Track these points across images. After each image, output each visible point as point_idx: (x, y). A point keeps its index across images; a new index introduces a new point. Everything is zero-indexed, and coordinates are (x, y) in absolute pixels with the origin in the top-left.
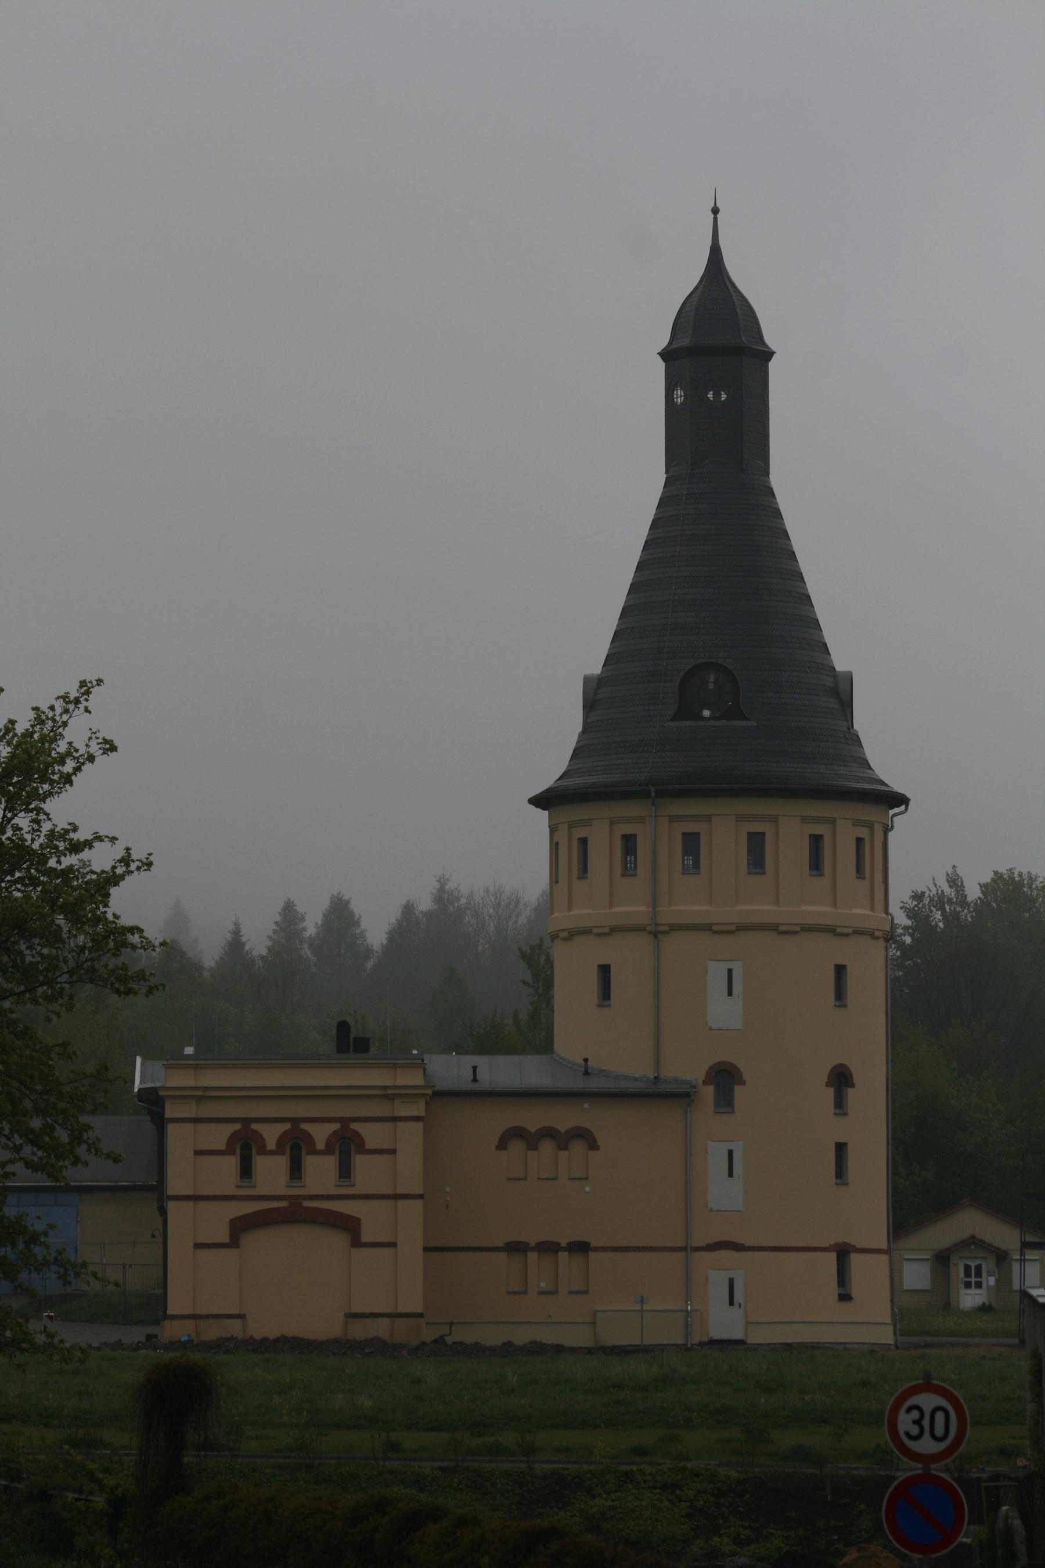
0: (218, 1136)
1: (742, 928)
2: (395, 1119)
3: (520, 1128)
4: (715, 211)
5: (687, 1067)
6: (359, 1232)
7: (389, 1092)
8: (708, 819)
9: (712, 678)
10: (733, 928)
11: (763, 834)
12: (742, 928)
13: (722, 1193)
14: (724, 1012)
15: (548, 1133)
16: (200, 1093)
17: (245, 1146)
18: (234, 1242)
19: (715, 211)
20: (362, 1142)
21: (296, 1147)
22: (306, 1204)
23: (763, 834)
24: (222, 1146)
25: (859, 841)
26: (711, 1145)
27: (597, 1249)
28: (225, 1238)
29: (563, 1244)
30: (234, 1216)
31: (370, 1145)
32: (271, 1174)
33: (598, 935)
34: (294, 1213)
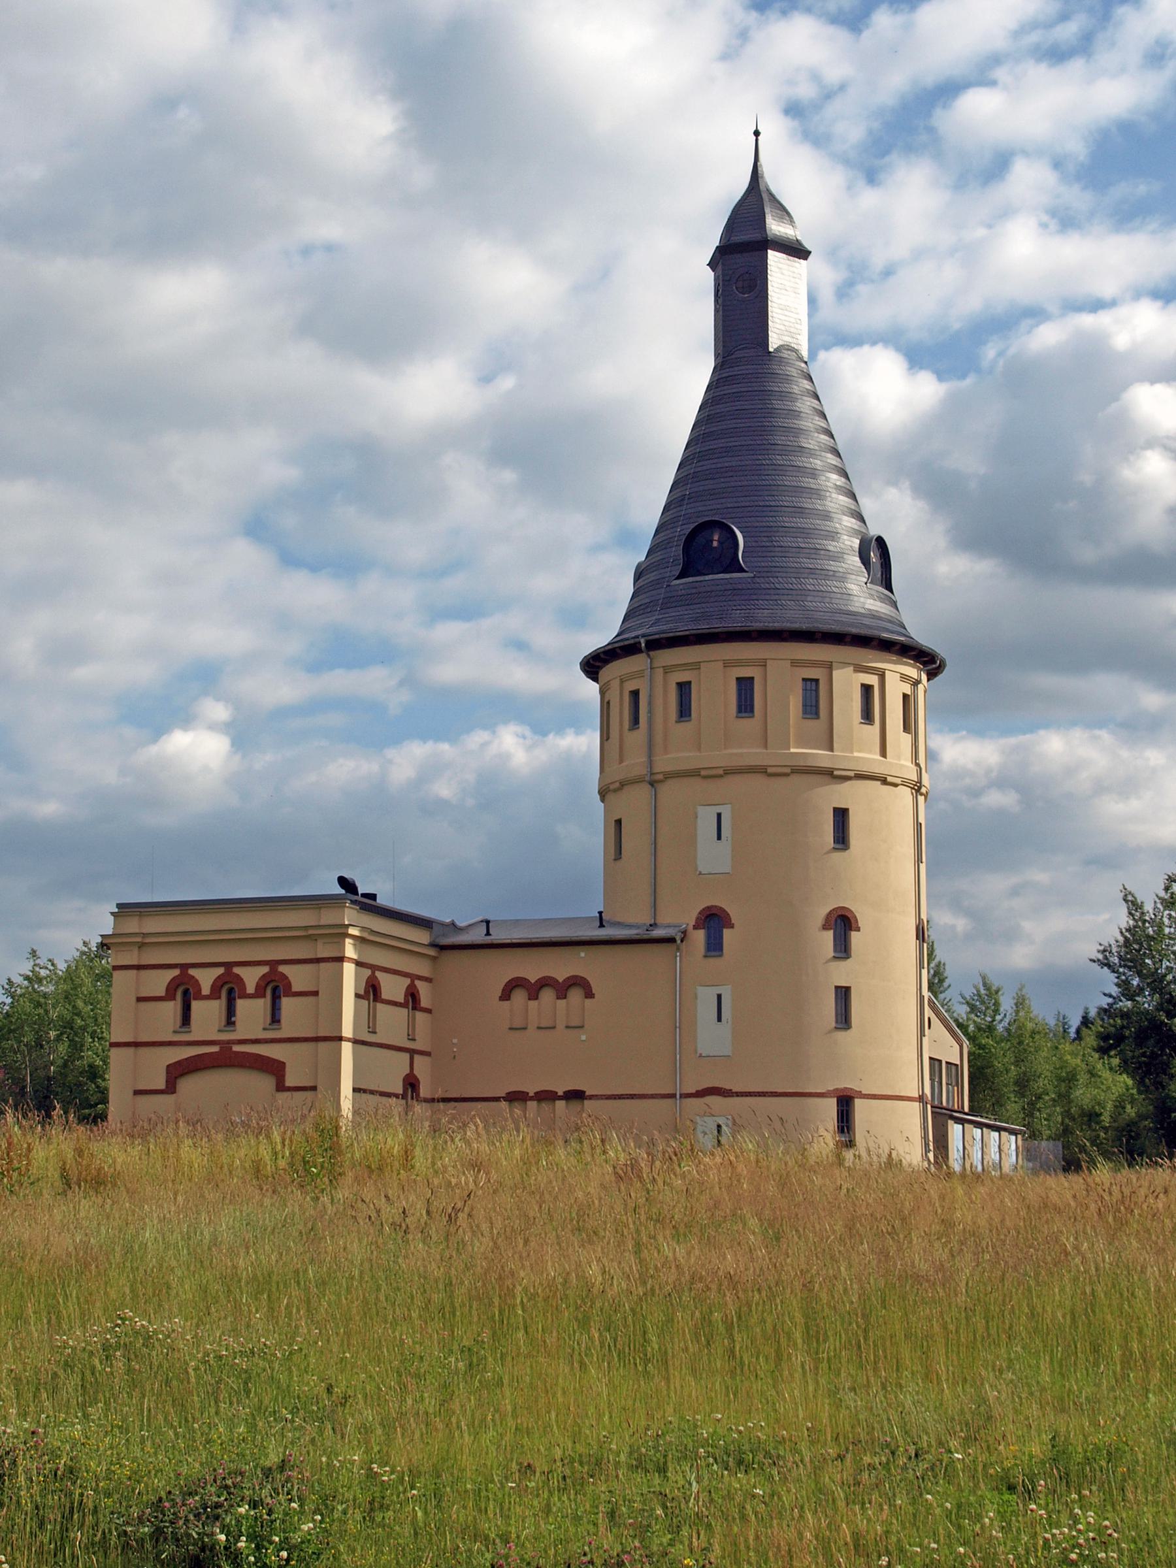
0: (158, 982)
1: (729, 772)
2: (318, 961)
3: (544, 978)
4: (757, 133)
5: (679, 914)
6: (284, 1076)
7: (311, 932)
8: (696, 666)
9: (716, 537)
10: (721, 772)
11: (752, 679)
12: (729, 772)
13: (712, 1038)
14: (713, 856)
15: (545, 982)
16: (139, 940)
17: (184, 991)
18: (171, 1088)
19: (757, 133)
20: (289, 985)
21: (229, 989)
22: (237, 1048)
23: (752, 679)
24: (162, 993)
25: (867, 689)
26: (700, 989)
27: (591, 1097)
28: (161, 1084)
29: (560, 1093)
30: (287, 1069)
31: (296, 988)
32: (207, 1015)
33: (615, 791)
34: (225, 1058)
